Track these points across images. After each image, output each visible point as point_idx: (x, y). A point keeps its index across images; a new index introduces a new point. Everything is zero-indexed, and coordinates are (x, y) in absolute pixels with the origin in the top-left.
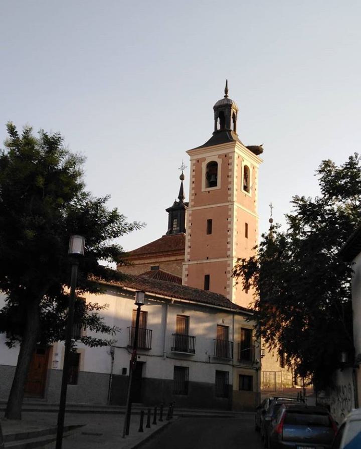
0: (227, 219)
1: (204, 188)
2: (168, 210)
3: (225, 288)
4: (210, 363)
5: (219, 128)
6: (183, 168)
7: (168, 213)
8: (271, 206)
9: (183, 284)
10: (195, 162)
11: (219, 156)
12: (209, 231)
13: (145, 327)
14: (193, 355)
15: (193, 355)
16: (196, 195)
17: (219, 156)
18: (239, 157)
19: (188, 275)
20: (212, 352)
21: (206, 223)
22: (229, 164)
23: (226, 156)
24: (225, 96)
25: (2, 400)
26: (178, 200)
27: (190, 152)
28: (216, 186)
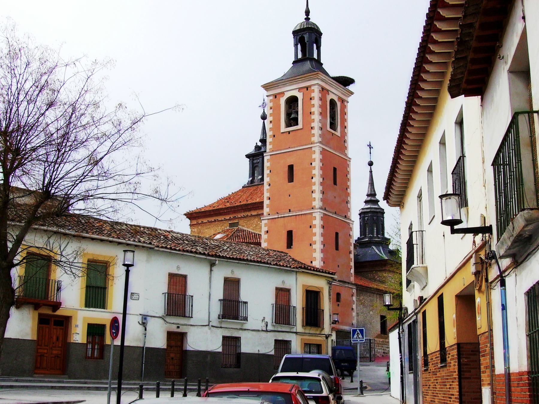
0: (311, 164)
1: (283, 128)
2: (248, 156)
3: (311, 245)
4: (267, 331)
5: (300, 56)
6: (264, 105)
7: (248, 160)
8: (370, 147)
9: (264, 245)
12: (291, 178)
13: (289, 304)
17: (300, 89)
19: (267, 232)
20: (269, 316)
21: (286, 169)
22: (311, 99)
24: (305, 19)
26: (260, 144)
28: (297, 124)
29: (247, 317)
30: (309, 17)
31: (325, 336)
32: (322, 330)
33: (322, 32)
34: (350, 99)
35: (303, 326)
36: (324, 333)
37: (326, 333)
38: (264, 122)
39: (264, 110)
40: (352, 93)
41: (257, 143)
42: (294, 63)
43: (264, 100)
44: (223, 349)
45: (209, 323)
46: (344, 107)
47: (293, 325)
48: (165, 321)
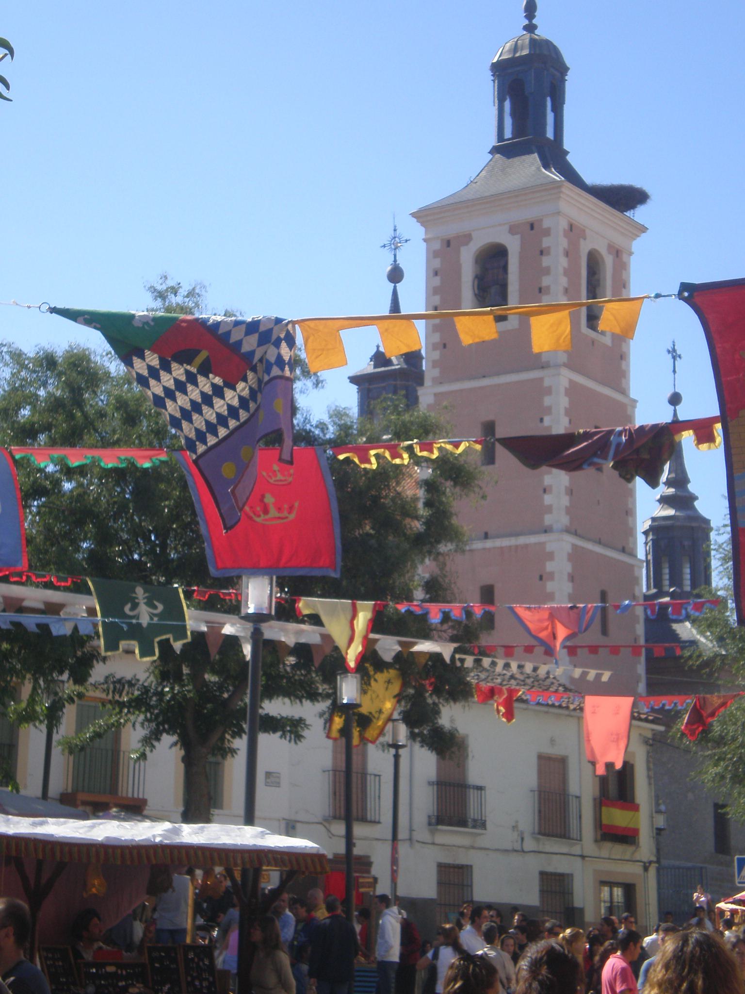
0: (542, 420)
5: (508, 134)
6: (395, 244)
8: (674, 354)
10: (437, 246)
11: (513, 230)
14: (483, 834)
15: (483, 834)
16: (445, 346)
17: (513, 230)
18: (571, 230)
20: (527, 819)
22: (542, 253)
23: (532, 227)
24: (526, 28)
25: (294, 991)
27: (423, 216)
29: (485, 821)
30: (534, 21)
31: (642, 864)
32: (635, 851)
33: (568, 65)
34: (638, 245)
35: (596, 841)
36: (638, 858)
37: (645, 860)
38: (395, 288)
39: (395, 256)
40: (643, 229)
41: (378, 347)
42: (495, 150)
43: (395, 230)
44: (439, 893)
45: (411, 835)
46: (621, 266)
47: (577, 840)
48: (329, 831)
